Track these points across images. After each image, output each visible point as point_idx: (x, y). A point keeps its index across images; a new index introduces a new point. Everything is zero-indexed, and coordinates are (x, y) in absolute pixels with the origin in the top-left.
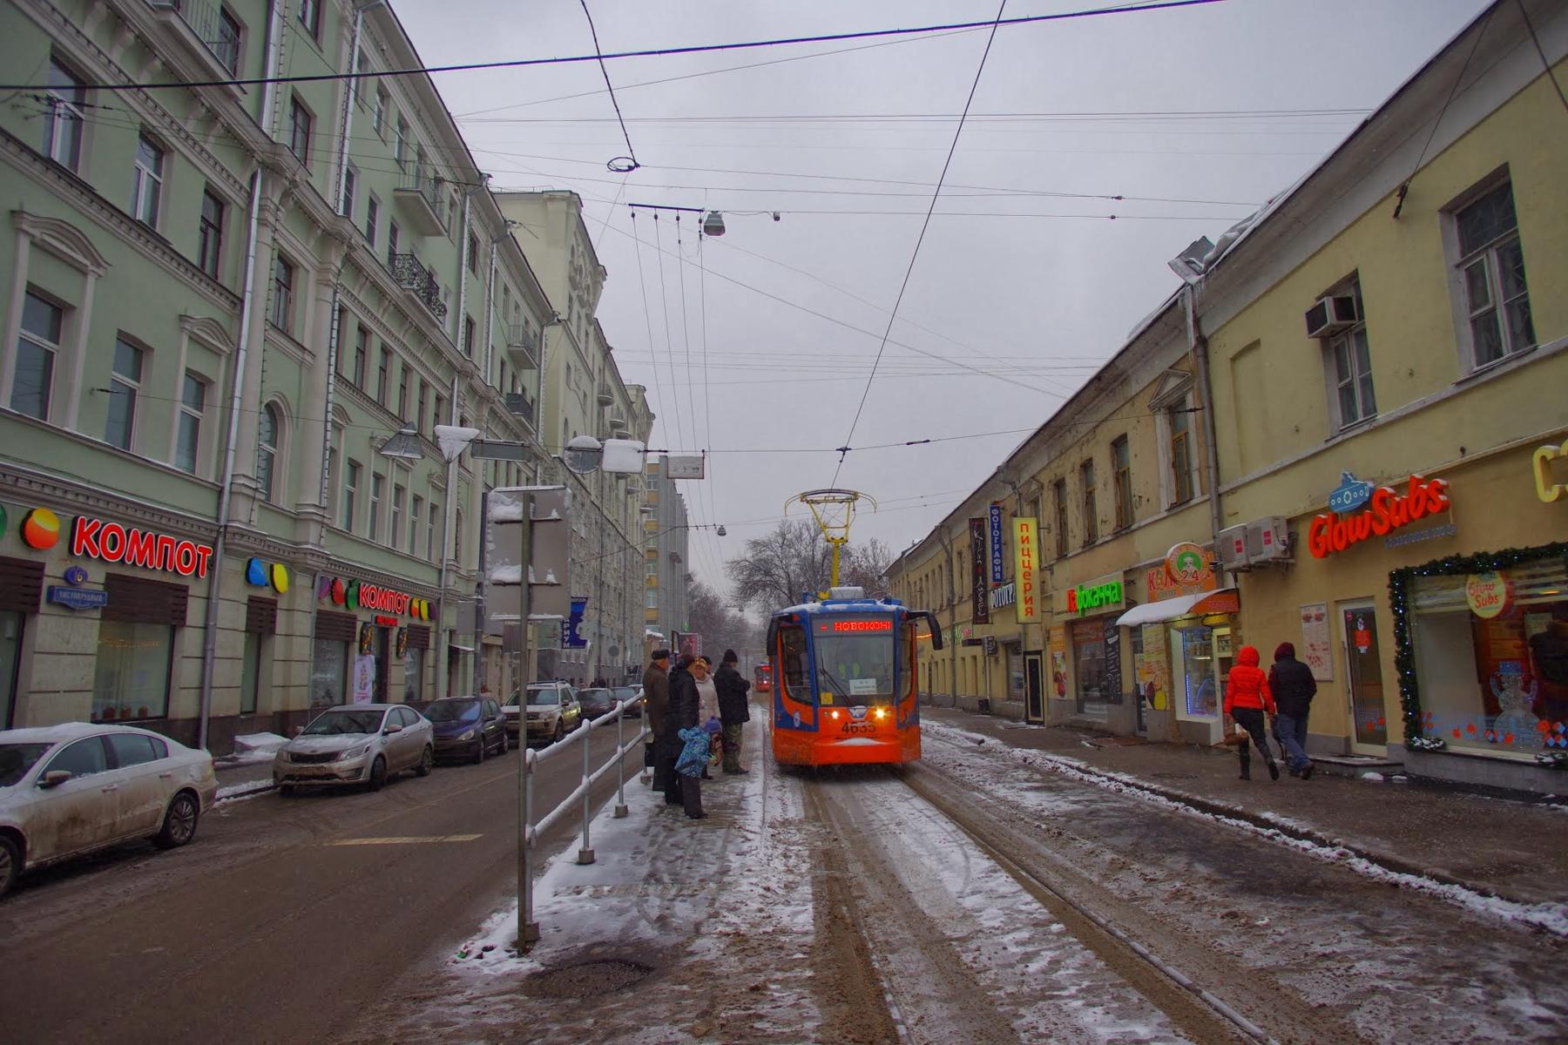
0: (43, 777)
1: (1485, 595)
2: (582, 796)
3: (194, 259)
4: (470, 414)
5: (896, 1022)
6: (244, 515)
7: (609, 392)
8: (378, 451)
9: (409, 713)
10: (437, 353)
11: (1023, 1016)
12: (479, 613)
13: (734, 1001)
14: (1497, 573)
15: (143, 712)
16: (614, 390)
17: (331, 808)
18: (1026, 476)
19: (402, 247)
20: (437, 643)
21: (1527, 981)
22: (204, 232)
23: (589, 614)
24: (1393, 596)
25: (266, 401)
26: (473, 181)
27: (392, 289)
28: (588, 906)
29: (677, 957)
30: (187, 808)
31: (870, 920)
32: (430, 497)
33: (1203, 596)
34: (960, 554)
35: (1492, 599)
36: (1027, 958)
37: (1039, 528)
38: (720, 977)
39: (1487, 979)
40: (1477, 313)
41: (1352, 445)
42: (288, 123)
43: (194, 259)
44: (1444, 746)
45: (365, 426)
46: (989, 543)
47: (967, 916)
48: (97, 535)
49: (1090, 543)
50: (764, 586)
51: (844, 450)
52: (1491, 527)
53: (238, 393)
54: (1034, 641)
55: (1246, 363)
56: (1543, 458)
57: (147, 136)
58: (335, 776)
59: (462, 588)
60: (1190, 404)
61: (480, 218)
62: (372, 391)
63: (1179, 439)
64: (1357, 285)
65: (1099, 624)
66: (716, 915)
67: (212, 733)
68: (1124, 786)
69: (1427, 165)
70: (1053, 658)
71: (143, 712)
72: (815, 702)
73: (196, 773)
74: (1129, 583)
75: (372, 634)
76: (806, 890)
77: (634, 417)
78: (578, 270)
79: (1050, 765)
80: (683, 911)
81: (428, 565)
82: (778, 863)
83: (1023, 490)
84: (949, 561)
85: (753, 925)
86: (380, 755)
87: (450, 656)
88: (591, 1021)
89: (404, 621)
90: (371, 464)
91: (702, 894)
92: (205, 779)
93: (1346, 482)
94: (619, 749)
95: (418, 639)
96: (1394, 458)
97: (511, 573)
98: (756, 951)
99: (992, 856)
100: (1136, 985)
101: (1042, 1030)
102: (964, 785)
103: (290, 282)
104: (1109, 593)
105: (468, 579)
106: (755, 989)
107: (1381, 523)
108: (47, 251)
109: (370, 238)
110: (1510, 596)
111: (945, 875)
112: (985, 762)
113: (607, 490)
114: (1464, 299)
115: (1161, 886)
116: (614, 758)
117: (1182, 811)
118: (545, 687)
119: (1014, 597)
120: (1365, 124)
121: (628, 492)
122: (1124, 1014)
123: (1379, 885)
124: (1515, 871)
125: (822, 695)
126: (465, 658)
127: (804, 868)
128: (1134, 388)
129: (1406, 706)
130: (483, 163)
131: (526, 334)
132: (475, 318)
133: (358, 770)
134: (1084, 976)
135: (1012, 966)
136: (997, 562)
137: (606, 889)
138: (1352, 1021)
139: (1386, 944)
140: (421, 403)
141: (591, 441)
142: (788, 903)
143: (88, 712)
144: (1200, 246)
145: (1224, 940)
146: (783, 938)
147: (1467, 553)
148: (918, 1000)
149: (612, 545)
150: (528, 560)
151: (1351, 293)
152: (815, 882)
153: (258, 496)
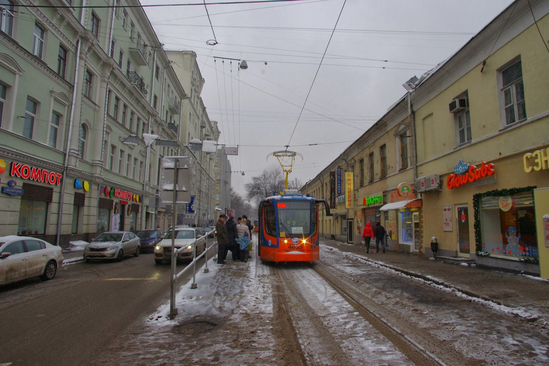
1: (505, 204)
6: (73, 163)
7: (205, 123)
10: (144, 107)
14: (509, 197)
16: (207, 123)
18: (350, 158)
19: (132, 69)
20: (142, 210)
22: (59, 61)
26: (157, 46)
27: (128, 84)
30: (52, 266)
32: (140, 159)
33: (409, 201)
34: (326, 184)
35: (507, 205)
45: (118, 133)
49: (371, 182)
50: (257, 193)
53: (72, 119)
55: (427, 121)
56: (527, 157)
59: (151, 191)
60: (408, 135)
62: (120, 121)
63: (404, 146)
64: (467, 95)
74: (385, 196)
75: (119, 207)
77: (213, 133)
78: (195, 80)
79: (355, 258)
81: (139, 183)
83: (349, 163)
84: (322, 186)
86: (121, 249)
89: (130, 203)
90: (119, 146)
92: (59, 256)
95: (135, 209)
97: (170, 187)
104: (377, 199)
109: (120, 65)
110: (513, 203)
114: (503, 101)
120: (473, 38)
121: (211, 159)
125: (281, 233)
128: (389, 128)
132: (157, 95)
133: (114, 254)
136: (339, 187)
137: (201, 297)
140: (138, 125)
144: (414, 79)
147: (500, 189)
150: (176, 182)
151: (465, 98)
153: (79, 157)
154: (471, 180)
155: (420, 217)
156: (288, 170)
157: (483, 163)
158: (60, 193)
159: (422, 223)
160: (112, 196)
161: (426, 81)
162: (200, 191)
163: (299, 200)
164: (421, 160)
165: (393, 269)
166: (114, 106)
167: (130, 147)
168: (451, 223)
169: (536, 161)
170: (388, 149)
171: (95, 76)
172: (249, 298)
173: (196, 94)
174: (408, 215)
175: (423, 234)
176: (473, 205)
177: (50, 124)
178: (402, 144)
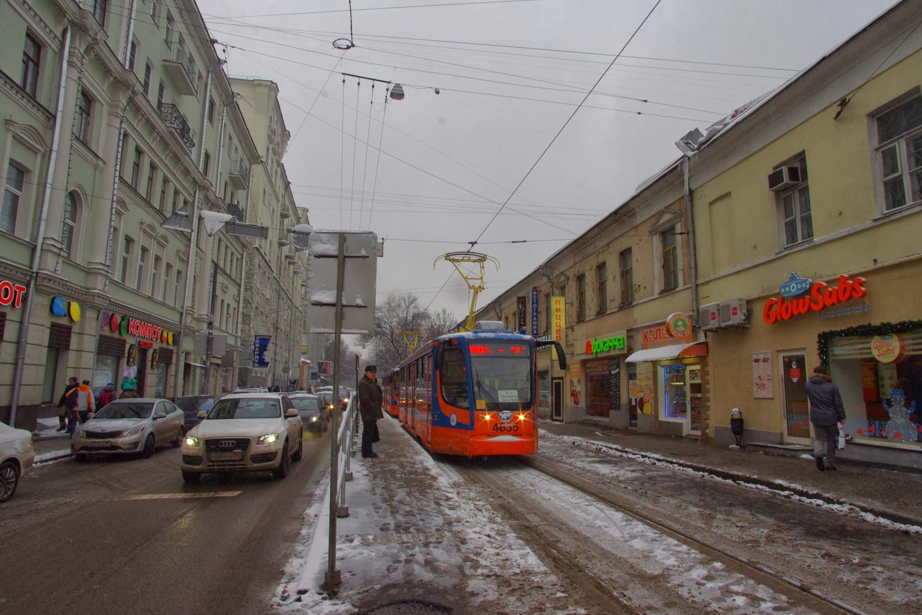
1: (885, 349)
3: (18, 80)
6: (50, 265)
10: (186, 172)
12: (210, 340)
17: (118, 470)
18: (557, 272)
19: (167, 99)
20: (178, 360)
22: (26, 63)
23: (270, 346)
24: (820, 349)
25: (70, 189)
26: (215, 64)
32: (177, 265)
33: (687, 346)
41: (794, 256)
43: (18, 80)
45: (137, 214)
49: (601, 312)
52: (892, 306)
55: (720, 207)
59: (194, 325)
62: (143, 192)
65: (604, 362)
70: (571, 382)
73: (20, 448)
74: (629, 337)
75: (136, 353)
79: (594, 447)
81: (174, 309)
83: (555, 281)
86: (151, 433)
87: (185, 369)
89: (157, 345)
90: (140, 240)
92: (27, 451)
93: (793, 278)
95: (165, 357)
97: (328, 297)
107: (817, 303)
109: (146, 86)
110: (902, 348)
114: (880, 168)
120: (824, 59)
121: (295, 273)
123: (894, 532)
125: (478, 402)
126: (195, 371)
128: (639, 220)
132: (211, 153)
133: (136, 444)
136: (535, 323)
137: (371, 537)
147: (876, 322)
150: (340, 288)
151: (797, 165)
153: (62, 253)
155: (704, 373)
156: (477, 286)
157: (842, 277)
158: (21, 323)
159: (708, 383)
160: (124, 332)
161: (721, 135)
162: (277, 328)
163: (510, 341)
164: (705, 272)
165: (688, 466)
166: (132, 165)
167: (159, 243)
168: (769, 385)
170: (636, 255)
171: (98, 105)
172: (473, 536)
174: (678, 371)
175: (709, 404)
176: (818, 352)
177: (4, 185)
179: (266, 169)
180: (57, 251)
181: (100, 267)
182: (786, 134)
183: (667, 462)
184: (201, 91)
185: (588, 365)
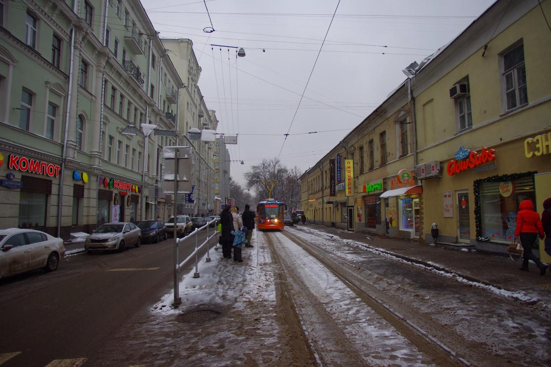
0: (3, 247)
1: (505, 189)
2: (195, 254)
3: (50, 60)
4: (153, 119)
5: (305, 331)
6: (71, 155)
7: (202, 113)
8: (120, 133)
9: (132, 225)
10: (141, 97)
11: (347, 329)
12: (157, 190)
13: (249, 324)
15: (37, 224)
16: (204, 112)
17: (106, 258)
18: (350, 145)
19: (127, 59)
21: (512, 316)
22: (54, 50)
23: (195, 191)
24: (475, 189)
25: (79, 114)
26: (153, 34)
28: (198, 292)
29: (229, 309)
30: (55, 258)
31: (295, 297)
32: (138, 149)
33: (410, 188)
34: (326, 172)
35: (507, 191)
36: (349, 310)
37: (354, 163)
38: (244, 316)
39: (499, 315)
40: (509, 91)
42: (84, 11)
43: (50, 60)
44: (489, 240)
45: (115, 124)
46: (336, 168)
47: (328, 296)
48: (18, 162)
49: (371, 169)
50: (257, 182)
51: (287, 135)
53: (68, 110)
54: (351, 203)
55: (428, 107)
56: (528, 142)
57: (30, 13)
58: (107, 247)
59: (150, 182)
60: (408, 121)
61: (156, 48)
62: (117, 111)
64: (468, 80)
65: (374, 197)
66: (242, 295)
67: (64, 232)
68: (380, 252)
69: (495, 38)
70: (358, 208)
71: (37, 224)
72: (265, 219)
73: (58, 246)
74: (385, 183)
76: (273, 287)
77: (211, 122)
78: (191, 68)
79: (356, 245)
80: (231, 294)
81: (138, 173)
82: (263, 278)
84: (322, 174)
85: (255, 298)
86: (122, 240)
88: (200, 330)
89: (130, 193)
90: (117, 137)
91: (237, 288)
92: (61, 248)
93: (461, 149)
94: (208, 238)
95: (135, 199)
96: (479, 141)
97: (171, 177)
98: (256, 307)
99: (336, 276)
100: (385, 318)
101: (353, 333)
102: (327, 252)
103: (86, 70)
105: (152, 179)
106: (256, 320)
108: (4, 62)
109: (116, 54)
111: (320, 282)
112: (334, 244)
113: (201, 147)
114: (505, 86)
115: (393, 286)
116: (206, 242)
117: (401, 261)
118: (180, 217)
119: (344, 187)
121: (209, 148)
122: (381, 328)
124: (510, 281)
126: (151, 206)
127: (272, 279)
128: (389, 115)
129: (477, 226)
130: (157, 28)
131: (173, 91)
132: (154, 85)
133: (115, 245)
134: (367, 316)
135: (343, 312)
136: (339, 175)
137: (204, 286)
138: (455, 329)
139: (467, 305)
140: (135, 115)
141: (196, 130)
142: (267, 291)
143: (17, 224)
145: (414, 304)
146: (265, 303)
147: (500, 175)
148: (312, 323)
149: (203, 167)
150: (177, 172)
151: (465, 83)
152: (276, 284)
153: (77, 148)
154: (472, 166)
155: (421, 203)
158: (59, 185)
159: (423, 209)
160: (111, 187)
165: (394, 255)
166: (110, 97)
167: (128, 138)
169: (537, 146)
170: (388, 135)
171: (90, 66)
173: (193, 83)
178: (402, 130)
179: (187, 90)
180: (74, 147)
181: (96, 153)
182: (459, 65)
183: (386, 253)
184: (147, 52)
185: (366, 199)
